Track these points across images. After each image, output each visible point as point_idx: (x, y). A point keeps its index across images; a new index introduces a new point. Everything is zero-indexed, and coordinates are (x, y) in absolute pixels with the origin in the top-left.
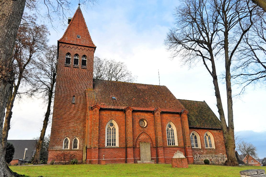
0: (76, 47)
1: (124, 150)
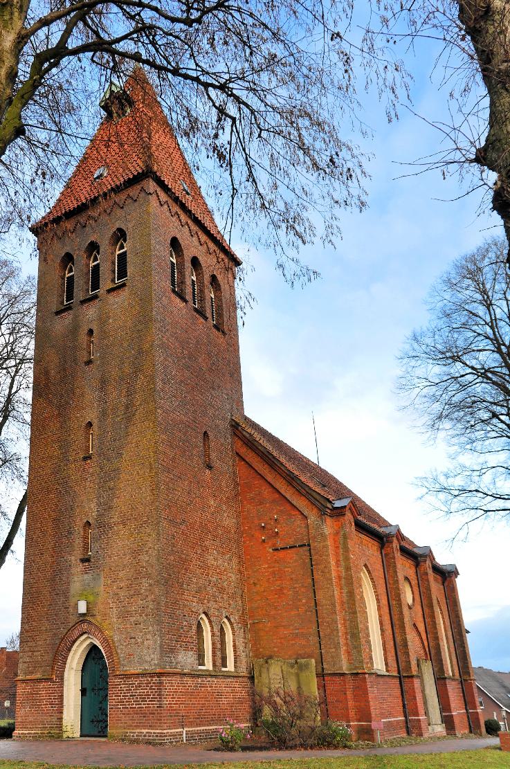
0: (194, 228)
1: (397, 681)
